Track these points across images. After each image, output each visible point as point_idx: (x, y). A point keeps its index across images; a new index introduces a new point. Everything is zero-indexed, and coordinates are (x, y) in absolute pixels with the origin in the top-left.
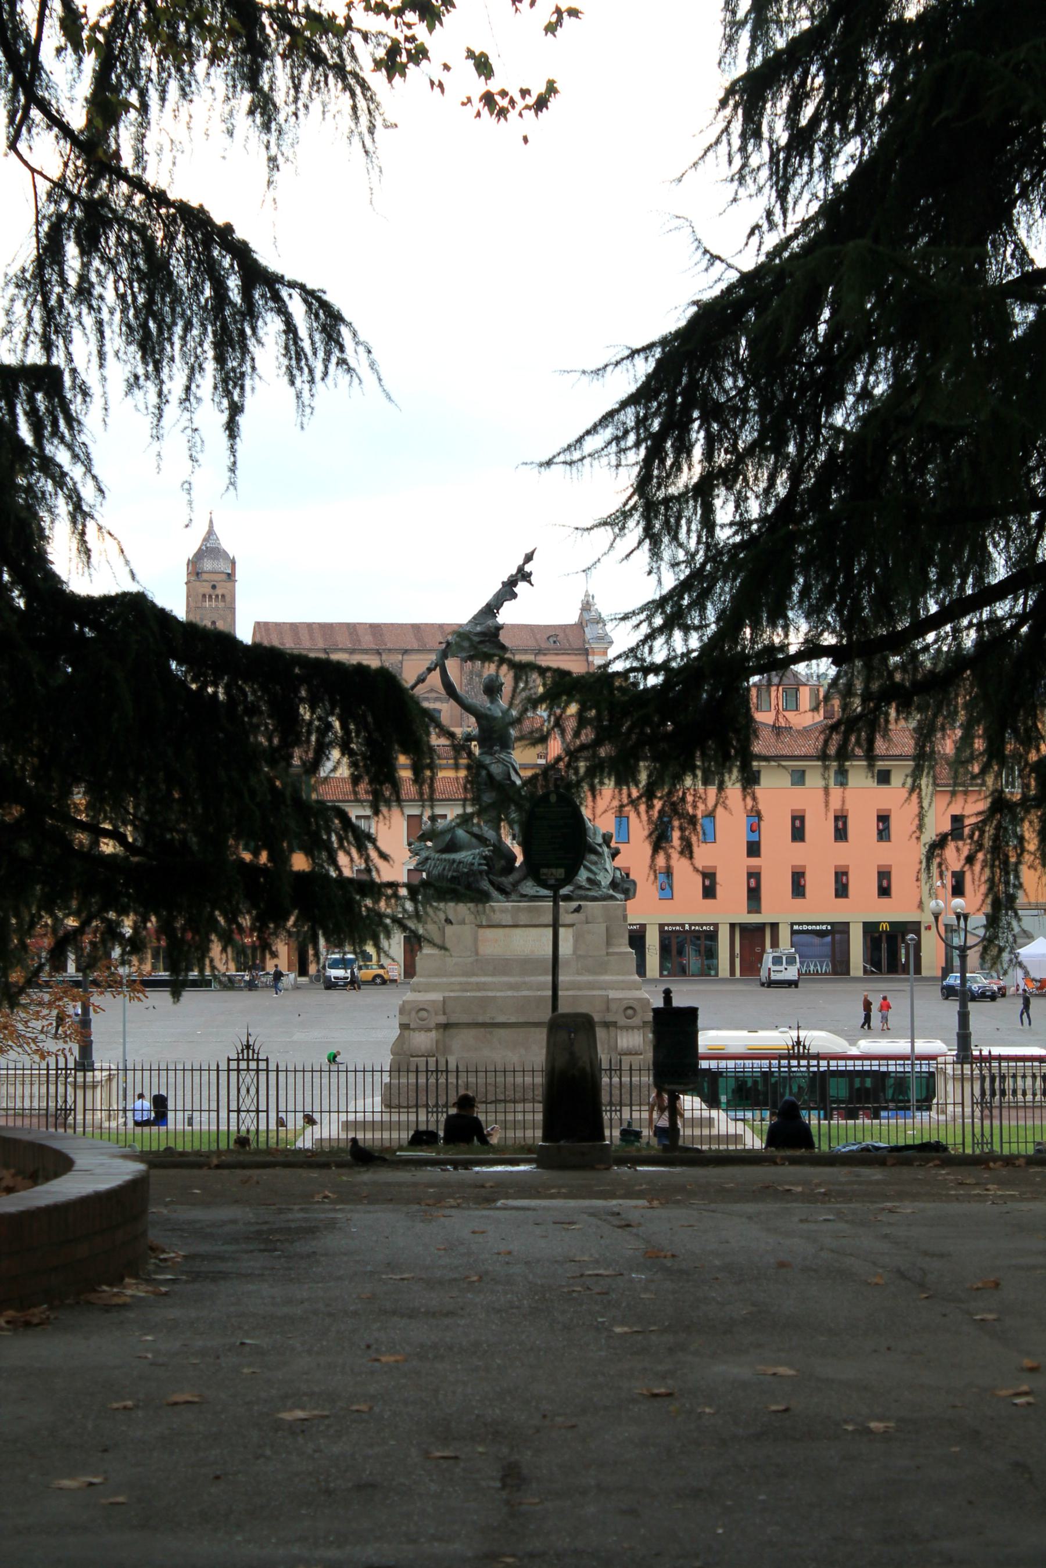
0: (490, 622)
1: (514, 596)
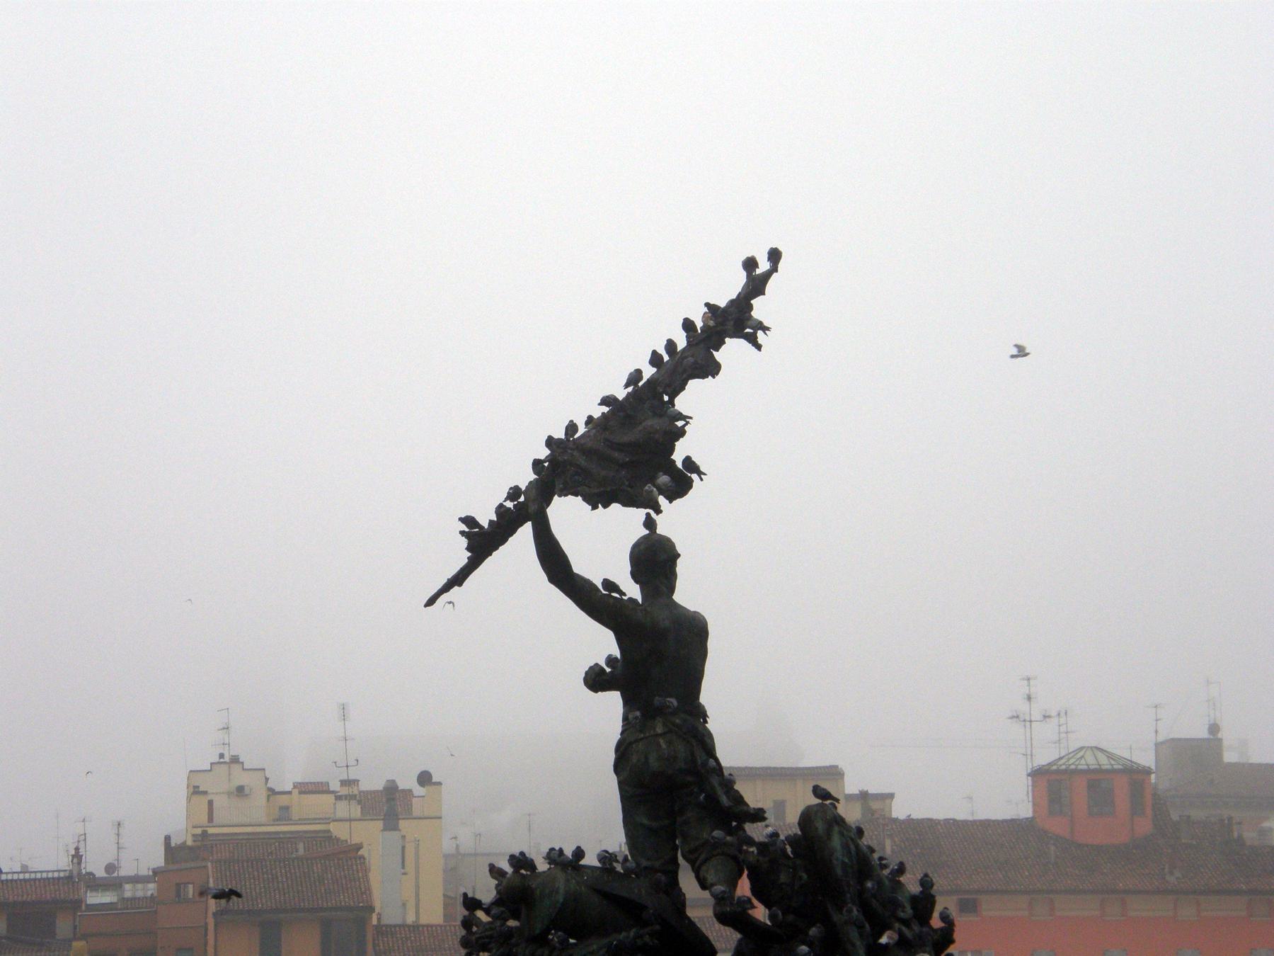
0: (653, 423)
1: (710, 369)
